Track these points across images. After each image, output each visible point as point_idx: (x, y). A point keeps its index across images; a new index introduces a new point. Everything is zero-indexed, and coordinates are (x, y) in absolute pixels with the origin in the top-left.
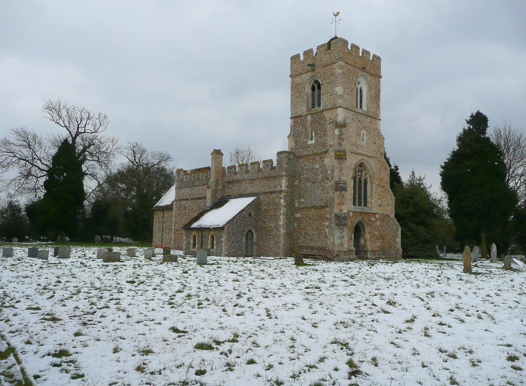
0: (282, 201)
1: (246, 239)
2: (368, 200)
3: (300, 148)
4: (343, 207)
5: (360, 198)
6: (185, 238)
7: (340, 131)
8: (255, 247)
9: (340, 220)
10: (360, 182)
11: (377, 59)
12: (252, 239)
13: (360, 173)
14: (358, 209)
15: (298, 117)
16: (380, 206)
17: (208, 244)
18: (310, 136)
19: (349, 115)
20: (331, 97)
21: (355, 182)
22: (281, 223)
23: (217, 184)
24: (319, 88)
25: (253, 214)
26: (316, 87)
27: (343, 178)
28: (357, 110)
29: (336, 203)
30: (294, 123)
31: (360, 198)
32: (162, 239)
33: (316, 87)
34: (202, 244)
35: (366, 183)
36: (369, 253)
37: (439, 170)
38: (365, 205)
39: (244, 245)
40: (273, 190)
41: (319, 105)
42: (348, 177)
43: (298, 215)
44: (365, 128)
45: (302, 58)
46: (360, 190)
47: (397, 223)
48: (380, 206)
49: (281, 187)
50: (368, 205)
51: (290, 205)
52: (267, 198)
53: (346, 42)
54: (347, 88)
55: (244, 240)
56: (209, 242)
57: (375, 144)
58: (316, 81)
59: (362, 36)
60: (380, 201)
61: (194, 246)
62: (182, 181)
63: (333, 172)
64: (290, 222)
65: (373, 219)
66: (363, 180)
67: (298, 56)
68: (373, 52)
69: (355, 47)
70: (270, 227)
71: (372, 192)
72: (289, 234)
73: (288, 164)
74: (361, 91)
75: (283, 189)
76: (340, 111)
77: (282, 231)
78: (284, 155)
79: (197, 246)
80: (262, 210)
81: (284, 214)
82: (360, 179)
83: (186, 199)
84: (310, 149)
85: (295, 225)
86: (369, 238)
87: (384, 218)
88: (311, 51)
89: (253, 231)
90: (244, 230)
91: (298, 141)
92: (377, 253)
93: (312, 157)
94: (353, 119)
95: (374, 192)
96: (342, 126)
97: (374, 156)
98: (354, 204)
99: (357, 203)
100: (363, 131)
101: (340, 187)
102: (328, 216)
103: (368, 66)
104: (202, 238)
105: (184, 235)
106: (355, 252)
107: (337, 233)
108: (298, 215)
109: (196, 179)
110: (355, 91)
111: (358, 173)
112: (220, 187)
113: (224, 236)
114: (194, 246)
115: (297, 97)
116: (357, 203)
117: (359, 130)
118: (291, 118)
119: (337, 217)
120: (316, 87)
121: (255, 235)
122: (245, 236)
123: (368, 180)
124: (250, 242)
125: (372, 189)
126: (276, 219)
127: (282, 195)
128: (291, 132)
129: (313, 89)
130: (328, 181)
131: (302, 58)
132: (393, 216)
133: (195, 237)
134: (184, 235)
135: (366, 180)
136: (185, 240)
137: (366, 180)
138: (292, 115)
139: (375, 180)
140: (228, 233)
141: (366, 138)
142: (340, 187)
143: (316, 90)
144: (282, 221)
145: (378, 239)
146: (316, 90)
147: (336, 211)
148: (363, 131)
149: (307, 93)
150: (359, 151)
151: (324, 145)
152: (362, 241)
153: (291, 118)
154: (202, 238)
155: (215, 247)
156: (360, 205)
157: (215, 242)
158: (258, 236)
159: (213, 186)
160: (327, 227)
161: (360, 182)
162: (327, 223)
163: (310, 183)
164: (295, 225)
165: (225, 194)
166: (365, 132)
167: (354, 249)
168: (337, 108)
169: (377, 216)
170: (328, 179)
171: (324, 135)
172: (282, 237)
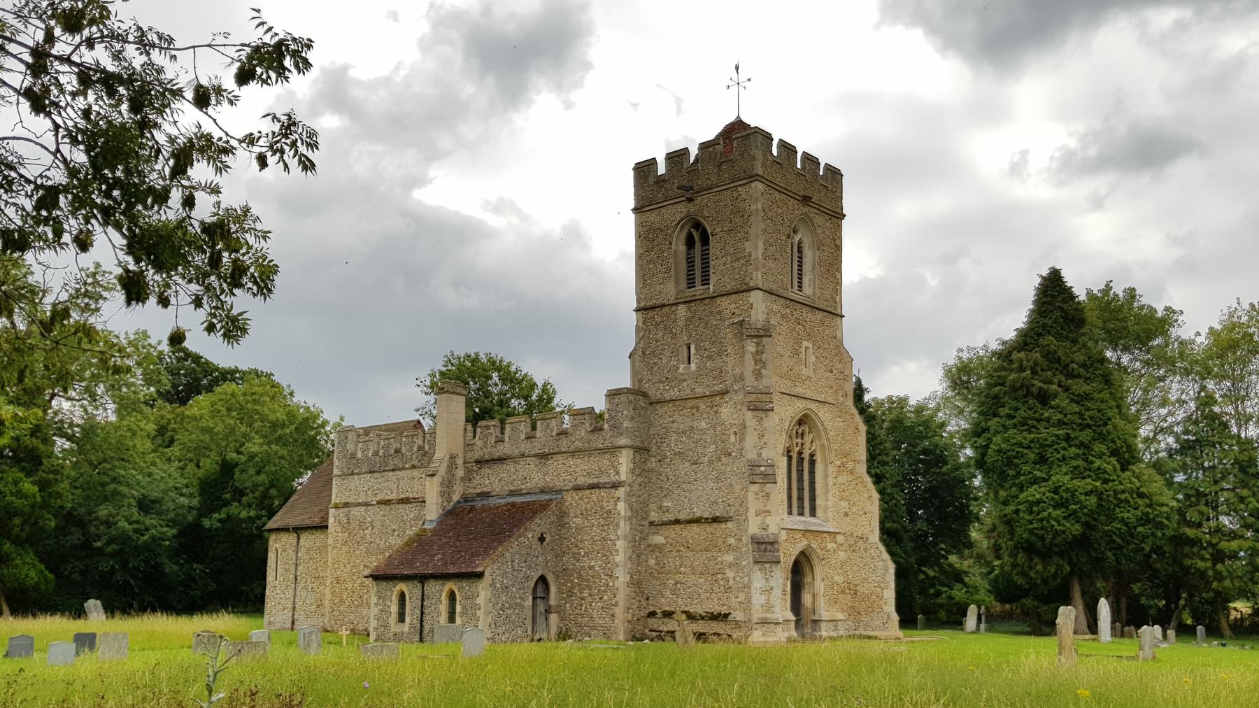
0: (621, 506)
1: (534, 599)
2: (819, 502)
3: (661, 382)
4: (768, 520)
5: (801, 499)
6: (374, 600)
7: (758, 344)
8: (553, 618)
9: (765, 548)
10: (801, 460)
11: (834, 174)
12: (546, 598)
13: (799, 440)
14: (796, 521)
15: (653, 308)
16: (846, 515)
17: (439, 614)
18: (686, 354)
19: (775, 308)
20: (735, 264)
21: (790, 458)
22: (620, 558)
23: (452, 464)
24: (705, 239)
25: (548, 539)
26: (696, 237)
27: (765, 454)
28: (792, 296)
29: (751, 513)
30: (644, 323)
31: (801, 499)
32: (294, 603)
33: (698, 236)
34: (422, 613)
35: (812, 463)
36: (823, 625)
37: (263, 367)
38: (813, 512)
39: (529, 614)
40: (595, 481)
41: (705, 281)
42: (775, 454)
43: (659, 539)
44: (809, 336)
45: (662, 169)
46: (800, 479)
47: (886, 556)
48: (846, 515)
49: (618, 473)
50: (819, 512)
51: (638, 513)
52: (581, 499)
53: (768, 137)
54: (771, 245)
55: (529, 602)
56: (444, 607)
57: (831, 371)
58: (698, 226)
59: (801, 123)
60: (844, 504)
61: (401, 618)
62: (353, 456)
63: (742, 439)
64: (638, 556)
65: (831, 546)
66: (806, 455)
67: (652, 162)
68: (825, 158)
69: (788, 149)
70: (591, 568)
71: (827, 484)
72: (637, 585)
73: (633, 418)
74: (800, 251)
75: (623, 477)
76: (756, 297)
77: (622, 577)
78: (623, 398)
79: (408, 619)
80: (569, 528)
81: (625, 538)
82: (800, 453)
83: (366, 504)
84: (685, 384)
85: (652, 562)
86: (822, 591)
87: (855, 543)
88: (684, 152)
89: (550, 578)
90: (527, 578)
91: (655, 364)
92: (841, 626)
93: (690, 403)
94: (783, 317)
95: (831, 483)
96: (762, 334)
97: (830, 400)
98: (790, 513)
99: (807, 510)
100: (805, 344)
101: (762, 473)
102: (731, 541)
103: (813, 193)
104: (423, 600)
105: (372, 594)
106: (793, 624)
107: (758, 580)
108: (659, 539)
109: (392, 452)
110: (789, 250)
111: (795, 440)
112: (460, 473)
113: (482, 594)
114: (401, 618)
115: (651, 261)
116: (807, 510)
117: (798, 341)
118: (637, 310)
119: (758, 542)
120: (696, 237)
121: (553, 589)
122: (530, 591)
123: (818, 458)
124: (541, 607)
125: (826, 476)
126: (606, 550)
127: (621, 492)
128: (637, 343)
129: (690, 243)
130: (730, 460)
131: (662, 169)
132: (875, 536)
133: (402, 597)
134: (372, 594)
135: (812, 455)
136: (377, 604)
137: (812, 455)
138: (638, 301)
139: (832, 456)
140: (493, 584)
141: (813, 359)
142: (760, 475)
143: (698, 245)
144: (621, 554)
145: (843, 592)
146: (698, 245)
147: (754, 528)
148: (805, 344)
149: (676, 252)
150: (799, 390)
151: (719, 374)
152: (807, 599)
153: (637, 310)
154: (423, 600)
155: (458, 620)
156: (801, 514)
157: (458, 608)
158: (560, 591)
159: (442, 470)
160: (731, 566)
161: (801, 460)
162: (729, 558)
163: (687, 464)
164: (652, 562)
165: (471, 490)
166: (810, 345)
167: (793, 618)
168: (749, 290)
169: (840, 539)
170: (730, 454)
171: (719, 353)
172: (621, 591)
